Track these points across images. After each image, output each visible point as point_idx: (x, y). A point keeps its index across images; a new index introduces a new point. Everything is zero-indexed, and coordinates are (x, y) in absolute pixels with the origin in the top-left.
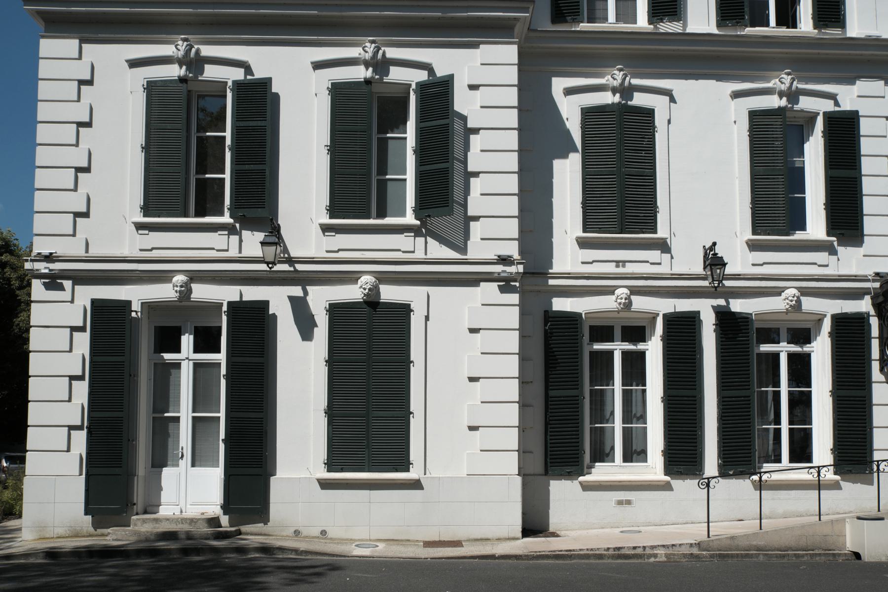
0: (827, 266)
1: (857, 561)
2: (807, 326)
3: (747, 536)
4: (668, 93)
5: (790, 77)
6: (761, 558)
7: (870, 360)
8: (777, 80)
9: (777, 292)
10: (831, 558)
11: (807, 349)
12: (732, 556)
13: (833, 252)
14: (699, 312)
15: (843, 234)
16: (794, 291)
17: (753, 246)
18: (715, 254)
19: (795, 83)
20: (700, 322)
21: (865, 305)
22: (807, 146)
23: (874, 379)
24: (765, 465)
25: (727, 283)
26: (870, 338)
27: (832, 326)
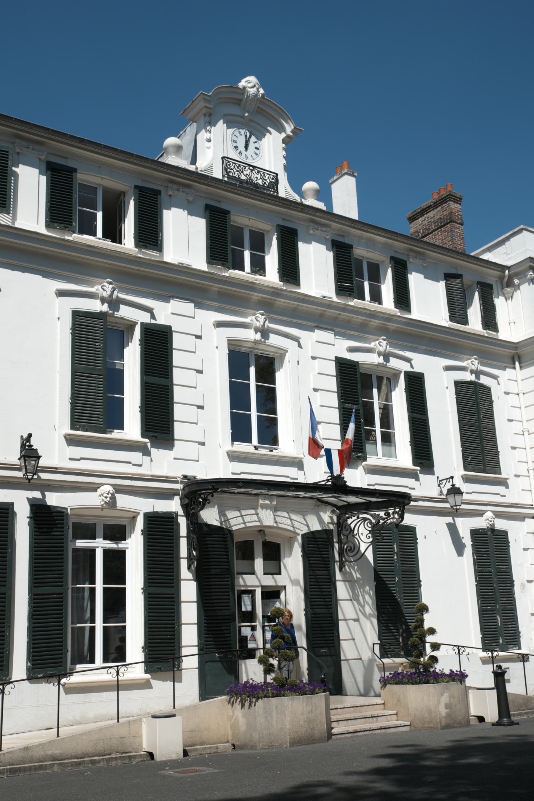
0: (141, 465)
1: (152, 762)
2: (123, 523)
3: (42, 745)
4: (296, 339)
5: (111, 286)
6: (56, 769)
7: (178, 558)
8: (100, 287)
9: (93, 488)
10: (127, 761)
11: (122, 545)
12: (24, 770)
13: (146, 453)
14: (12, 504)
15: (155, 437)
16: (110, 488)
17: (71, 441)
18: (31, 446)
19: (116, 292)
20: (14, 514)
21: (174, 506)
22: (126, 350)
23: (182, 577)
24: (78, 666)
25: (44, 476)
26: (178, 537)
27: (144, 524)
